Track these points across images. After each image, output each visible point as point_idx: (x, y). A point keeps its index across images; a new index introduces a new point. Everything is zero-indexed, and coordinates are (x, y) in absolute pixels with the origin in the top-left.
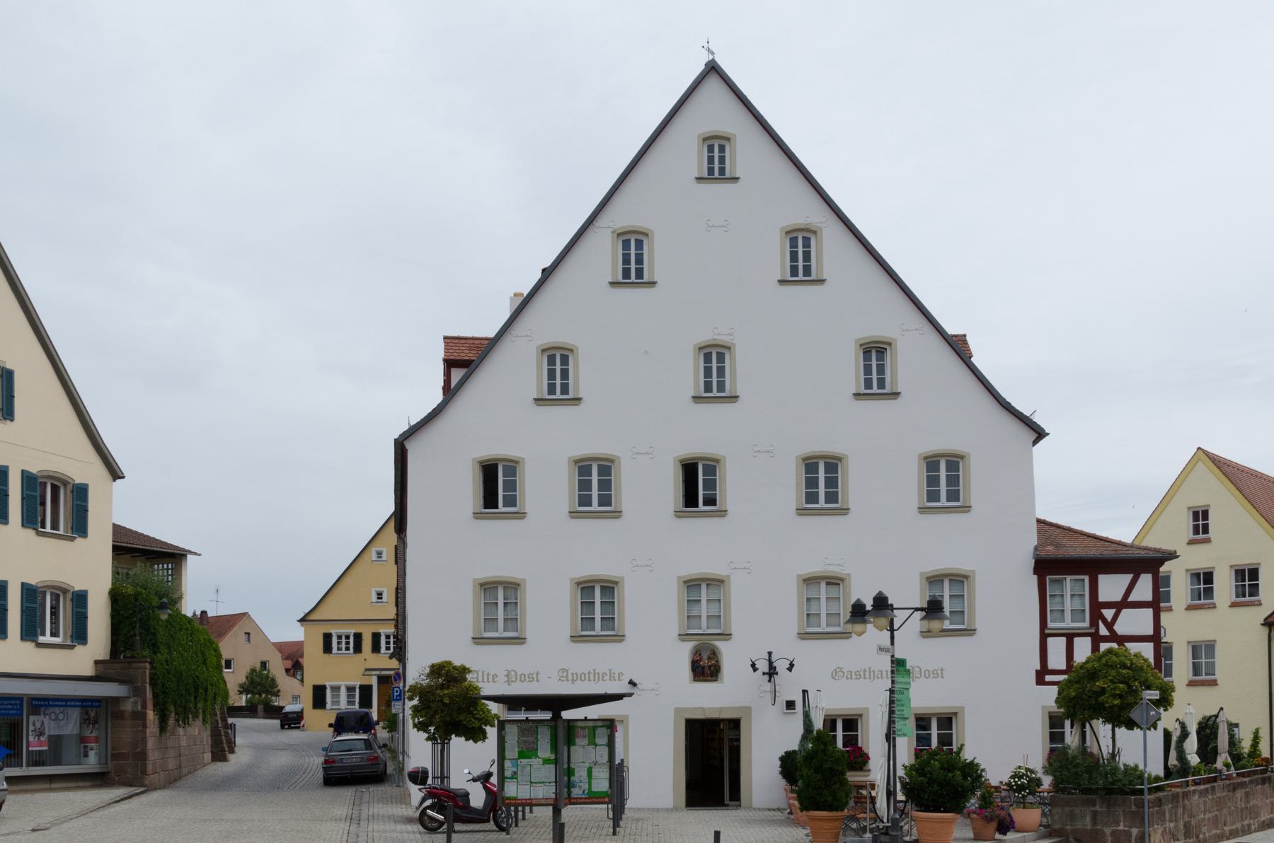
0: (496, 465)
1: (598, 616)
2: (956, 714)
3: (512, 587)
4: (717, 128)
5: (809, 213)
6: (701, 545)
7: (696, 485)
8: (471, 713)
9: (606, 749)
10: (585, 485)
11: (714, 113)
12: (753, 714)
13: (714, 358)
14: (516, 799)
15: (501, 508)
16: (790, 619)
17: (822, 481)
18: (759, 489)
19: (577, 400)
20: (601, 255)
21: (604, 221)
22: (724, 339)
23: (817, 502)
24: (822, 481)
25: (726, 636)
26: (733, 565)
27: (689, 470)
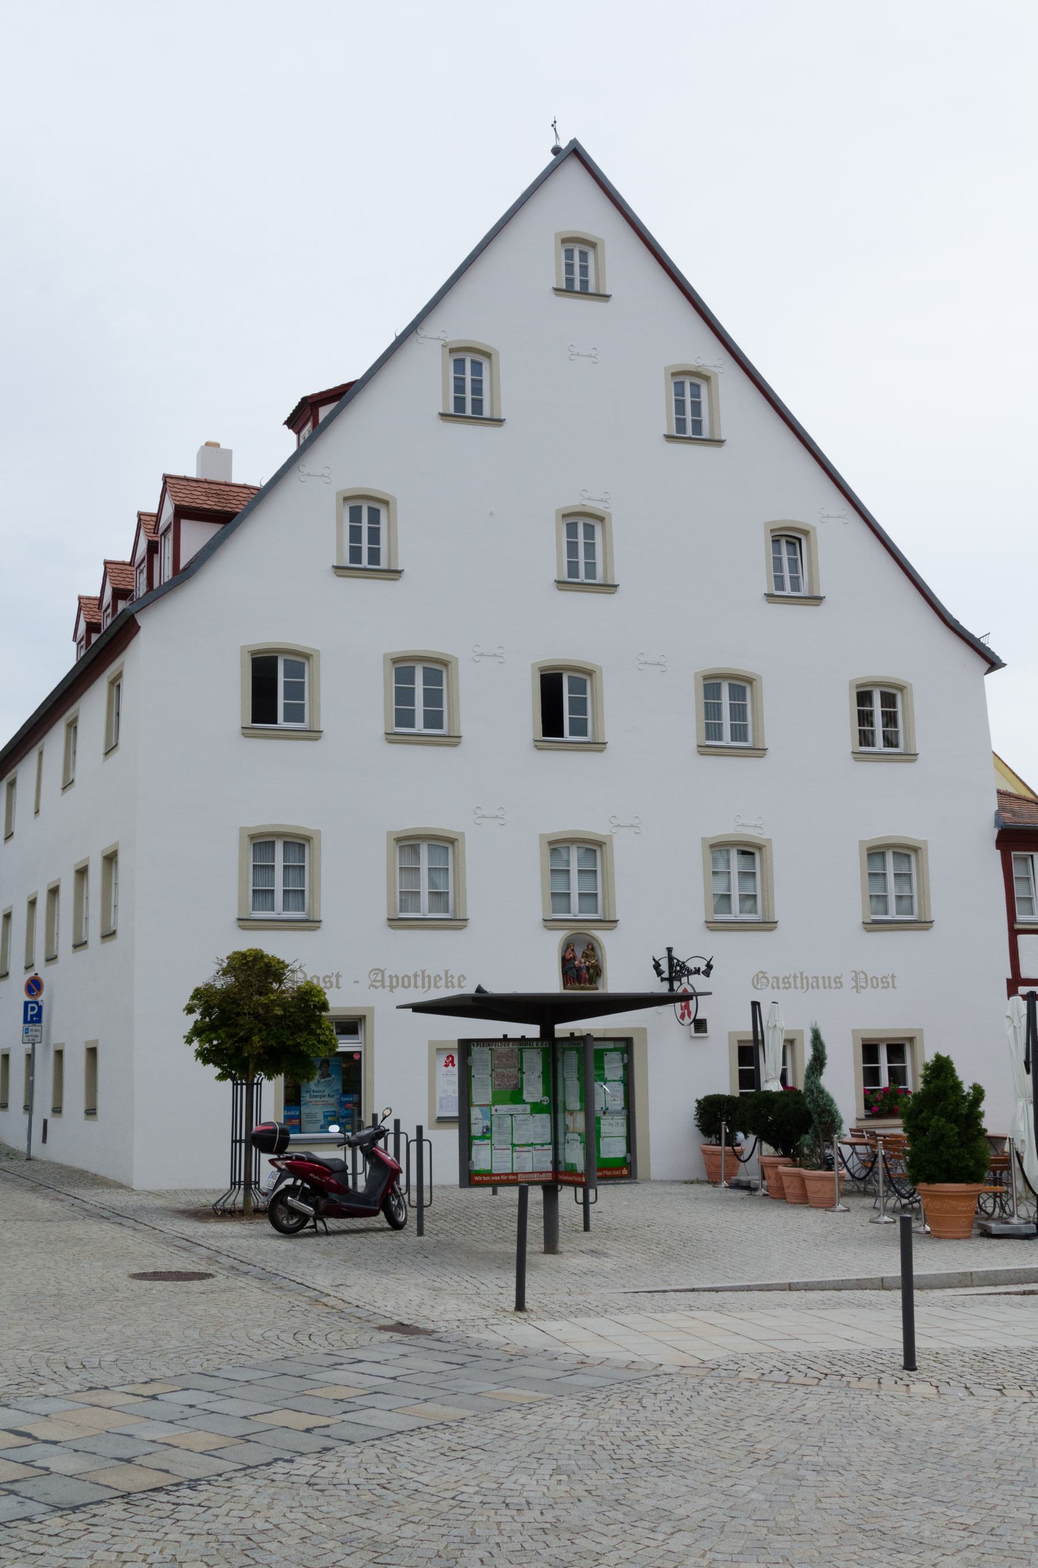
0: (275, 660)
1: (279, 887)
2: (911, 1040)
3: (298, 844)
4: (579, 226)
5: (702, 352)
6: (569, 790)
7: (559, 705)
8: (312, 1032)
9: (620, 1088)
10: (404, 696)
11: (575, 208)
12: (650, 1038)
13: (582, 528)
14: (489, 1174)
15: (567, 736)
16: (696, 905)
17: (728, 709)
18: (644, 713)
19: (395, 573)
20: (427, 376)
21: (432, 329)
22: (596, 506)
23: (413, 726)
24: (728, 709)
25: (610, 923)
26: (480, 813)
27: (550, 685)
